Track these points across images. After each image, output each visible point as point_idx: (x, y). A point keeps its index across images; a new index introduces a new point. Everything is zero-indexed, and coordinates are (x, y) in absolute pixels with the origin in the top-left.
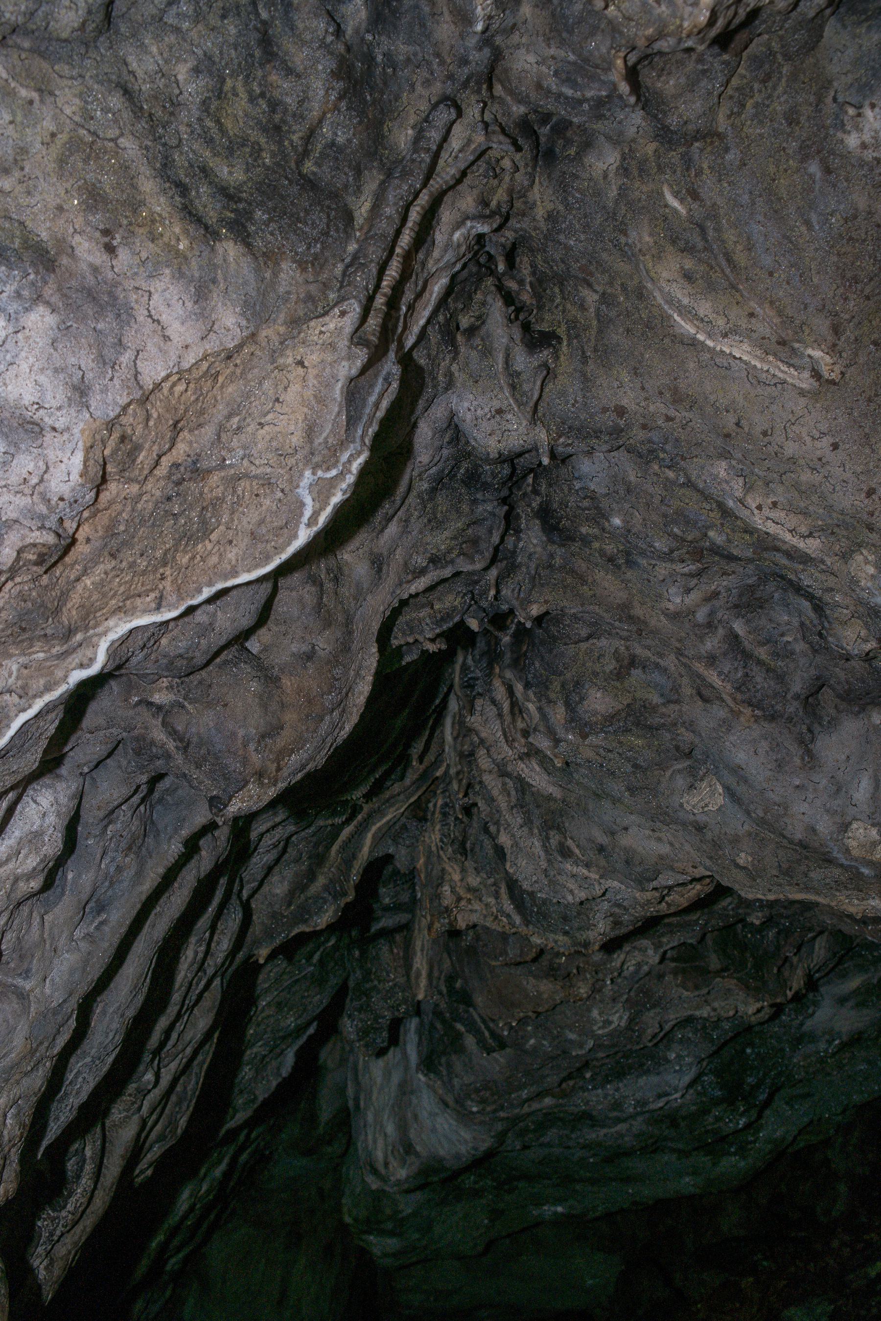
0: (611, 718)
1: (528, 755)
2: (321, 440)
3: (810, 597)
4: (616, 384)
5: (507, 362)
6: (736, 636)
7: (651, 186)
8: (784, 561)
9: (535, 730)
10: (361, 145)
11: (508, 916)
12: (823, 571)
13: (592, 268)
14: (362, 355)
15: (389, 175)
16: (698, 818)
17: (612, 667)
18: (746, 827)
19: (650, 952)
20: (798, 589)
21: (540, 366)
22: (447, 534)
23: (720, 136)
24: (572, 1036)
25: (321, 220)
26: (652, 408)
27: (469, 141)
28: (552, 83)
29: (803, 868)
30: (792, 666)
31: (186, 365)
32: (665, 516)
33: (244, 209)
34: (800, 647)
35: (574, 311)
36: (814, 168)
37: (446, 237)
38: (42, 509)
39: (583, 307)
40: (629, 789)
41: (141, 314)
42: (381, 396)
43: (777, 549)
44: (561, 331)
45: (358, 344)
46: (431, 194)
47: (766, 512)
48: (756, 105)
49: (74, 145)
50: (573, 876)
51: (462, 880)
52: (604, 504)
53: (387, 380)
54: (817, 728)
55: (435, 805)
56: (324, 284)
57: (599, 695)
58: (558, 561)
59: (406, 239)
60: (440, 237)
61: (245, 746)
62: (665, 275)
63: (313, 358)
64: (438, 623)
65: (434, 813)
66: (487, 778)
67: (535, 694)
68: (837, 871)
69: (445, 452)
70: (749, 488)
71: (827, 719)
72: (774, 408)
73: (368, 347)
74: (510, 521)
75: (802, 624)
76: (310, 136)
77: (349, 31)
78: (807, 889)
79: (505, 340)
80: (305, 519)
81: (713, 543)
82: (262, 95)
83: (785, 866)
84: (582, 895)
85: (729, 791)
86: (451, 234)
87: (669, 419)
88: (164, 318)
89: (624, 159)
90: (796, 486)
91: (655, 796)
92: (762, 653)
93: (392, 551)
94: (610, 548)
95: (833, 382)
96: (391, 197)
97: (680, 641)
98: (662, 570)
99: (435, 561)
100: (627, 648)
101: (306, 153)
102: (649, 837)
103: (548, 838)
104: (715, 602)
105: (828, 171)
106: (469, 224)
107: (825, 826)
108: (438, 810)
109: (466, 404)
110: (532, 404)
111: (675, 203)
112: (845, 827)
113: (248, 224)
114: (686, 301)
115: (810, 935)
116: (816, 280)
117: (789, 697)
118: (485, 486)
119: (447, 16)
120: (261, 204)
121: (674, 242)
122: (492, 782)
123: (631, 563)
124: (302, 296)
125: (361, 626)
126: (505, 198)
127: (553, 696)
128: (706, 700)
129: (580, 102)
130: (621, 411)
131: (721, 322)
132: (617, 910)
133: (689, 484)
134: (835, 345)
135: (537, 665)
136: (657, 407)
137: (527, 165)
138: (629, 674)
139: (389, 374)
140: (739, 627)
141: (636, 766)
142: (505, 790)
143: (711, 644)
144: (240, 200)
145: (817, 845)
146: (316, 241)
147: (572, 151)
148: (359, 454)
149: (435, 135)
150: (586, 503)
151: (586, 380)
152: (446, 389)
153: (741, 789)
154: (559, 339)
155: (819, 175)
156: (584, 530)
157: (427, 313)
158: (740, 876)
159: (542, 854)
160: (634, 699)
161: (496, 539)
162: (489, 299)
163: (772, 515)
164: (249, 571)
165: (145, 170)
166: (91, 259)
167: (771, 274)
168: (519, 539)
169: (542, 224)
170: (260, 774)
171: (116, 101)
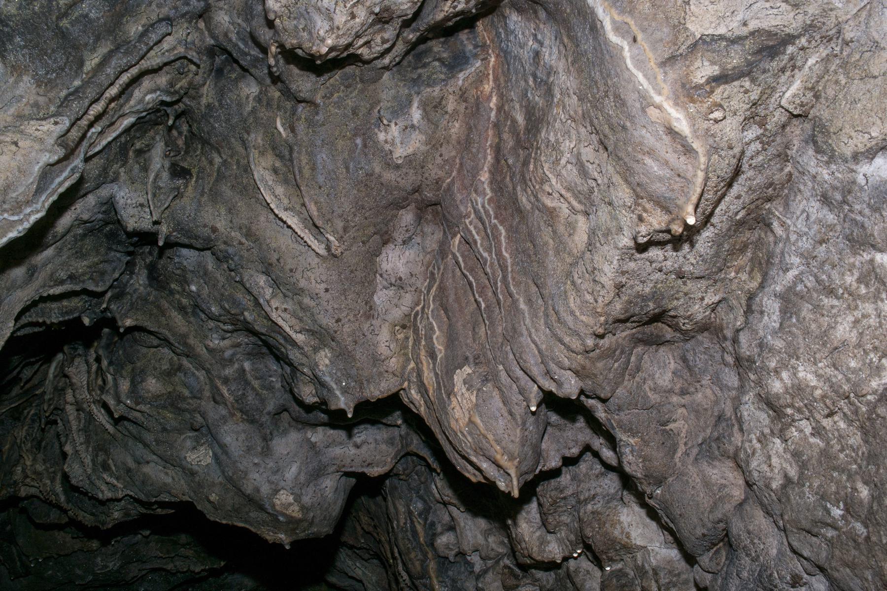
0: (157, 397)
2: (14, 195)
4: (217, 213)
5: (155, 179)
6: (244, 371)
7: (271, 114)
8: (282, 341)
10: (105, 24)
12: (302, 354)
13: (224, 144)
14: (61, 152)
15: (118, 48)
16: (194, 467)
17: (166, 367)
18: (220, 479)
21: (174, 188)
22: (85, 263)
23: (316, 105)
24: (79, 572)
25: (62, 59)
26: (233, 234)
27: (174, 48)
28: (234, 37)
29: (247, 509)
30: (271, 395)
32: (222, 295)
33: (8, 33)
35: (204, 162)
36: (359, 141)
37: (142, 95)
39: (211, 163)
40: (156, 440)
42: (66, 179)
44: (194, 171)
45: (60, 145)
46: (140, 69)
47: (279, 312)
48: (339, 97)
50: (107, 483)
51: (32, 466)
52: (189, 276)
53: (73, 171)
54: (275, 433)
55: (28, 413)
56: (50, 99)
57: (154, 381)
58: (151, 298)
59: (113, 91)
60: (137, 94)
65: (25, 418)
67: (114, 370)
68: (265, 516)
69: (100, 216)
70: (274, 296)
71: (282, 428)
72: (300, 258)
73: (66, 149)
74: (130, 265)
78: (246, 522)
79: (159, 166)
83: (237, 506)
86: (146, 95)
87: (241, 243)
89: (260, 93)
90: (300, 303)
91: (171, 449)
92: (256, 384)
93: (45, 265)
94: (185, 301)
95: (335, 256)
96: (114, 62)
97: (211, 365)
99: (72, 277)
101: (65, 15)
103: (97, 456)
104: (237, 349)
106: (158, 93)
107: (265, 489)
108: (29, 416)
109: (122, 194)
110: (163, 208)
111: (281, 129)
112: (276, 491)
113: (8, 44)
116: (342, 200)
117: (265, 412)
118: (120, 243)
120: (22, 34)
121: (274, 149)
122: (70, 409)
124: (32, 102)
125: (6, 308)
126: (186, 85)
129: (246, 54)
130: (214, 230)
131: (286, 201)
133: (241, 282)
134: (342, 237)
135: (121, 352)
137: (204, 73)
138: (175, 375)
139: (76, 167)
140: (247, 365)
143: (228, 371)
144: (7, 25)
145: (258, 499)
146: (54, 71)
147: (233, 76)
148: (38, 212)
149: (154, 37)
150: (178, 272)
152: (112, 181)
153: (223, 457)
154: (191, 175)
155: (360, 146)
156: (173, 286)
157: (114, 135)
158: (209, 506)
159: (91, 464)
160: (174, 390)
162: (158, 138)
163: (282, 315)
167: (320, 187)
168: (131, 278)
169: (203, 108)
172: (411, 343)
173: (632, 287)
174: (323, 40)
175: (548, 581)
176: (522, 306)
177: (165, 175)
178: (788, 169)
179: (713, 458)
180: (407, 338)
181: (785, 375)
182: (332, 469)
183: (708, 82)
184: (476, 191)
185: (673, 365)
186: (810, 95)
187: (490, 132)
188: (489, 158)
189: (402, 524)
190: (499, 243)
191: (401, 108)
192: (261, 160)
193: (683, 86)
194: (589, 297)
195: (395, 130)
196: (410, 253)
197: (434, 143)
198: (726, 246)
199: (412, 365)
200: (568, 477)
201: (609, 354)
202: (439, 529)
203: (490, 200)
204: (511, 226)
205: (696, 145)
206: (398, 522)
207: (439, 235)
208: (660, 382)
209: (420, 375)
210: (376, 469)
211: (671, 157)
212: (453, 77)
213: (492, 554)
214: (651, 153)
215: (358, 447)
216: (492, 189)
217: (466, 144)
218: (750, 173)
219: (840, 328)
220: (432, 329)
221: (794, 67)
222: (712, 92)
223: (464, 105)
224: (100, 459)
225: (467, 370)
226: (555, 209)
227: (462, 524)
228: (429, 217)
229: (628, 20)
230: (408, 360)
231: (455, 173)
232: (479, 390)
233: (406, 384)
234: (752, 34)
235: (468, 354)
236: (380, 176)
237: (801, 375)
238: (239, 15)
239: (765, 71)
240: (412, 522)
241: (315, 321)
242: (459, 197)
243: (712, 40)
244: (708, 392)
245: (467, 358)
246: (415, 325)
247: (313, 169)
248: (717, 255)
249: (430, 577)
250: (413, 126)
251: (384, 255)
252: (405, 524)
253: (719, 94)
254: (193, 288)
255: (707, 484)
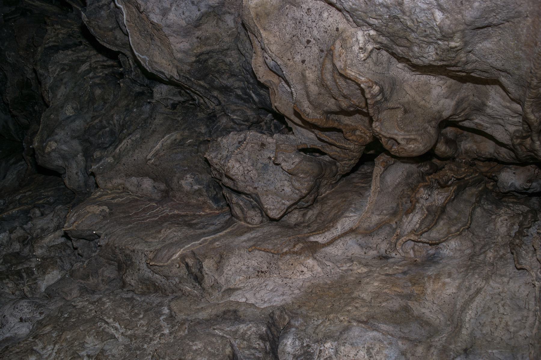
0: (93, 93)
1: (91, 67)
3: (108, 147)
6: (105, 128)
8: (116, 144)
9: (95, 74)
11: (48, 43)
19: (31, 76)
20: (110, 145)
24: (6, 44)
26: (153, 125)
31: (171, 45)
32: (132, 121)
34: (100, 141)
35: (178, 114)
36: (186, 168)
38: (148, 10)
39: (179, 116)
41: (183, 40)
43: (119, 143)
44: (175, 111)
47: (127, 143)
48: (201, 160)
49: (218, 38)
61: (97, 21)
62: (178, 136)
63: (170, 67)
64: (123, 62)
66: (88, 52)
70: (132, 140)
75: (104, 143)
76: (216, 77)
77: (236, 90)
80: (139, 55)
81: (124, 130)
82: (225, 71)
84: (50, 70)
85: (70, 117)
88: (182, 44)
89: (202, 133)
90: (130, 150)
92: (101, 133)
94: (131, 106)
96: (201, 89)
98: (122, 117)
100: (109, 102)
101: (213, 75)
102: (62, 94)
103: (67, 66)
105: (185, 170)
107: (57, 137)
111: (189, 141)
112: (56, 142)
114: (171, 138)
115: (29, 120)
119: (235, 108)
121: (183, 139)
123: (126, 110)
127: (102, 81)
128: (93, 117)
130: (155, 119)
131: (165, 144)
132: (44, 77)
133: (137, 129)
136: (153, 126)
140: (107, 129)
141: (80, 96)
142: (84, 56)
143: (104, 122)
151: (162, 113)
156: (136, 102)
159: (63, 62)
161: (138, 82)
164: (132, 40)
165: (212, 49)
166: (197, 33)
168: (138, 86)
170: (89, 22)
171: (225, 47)
172: (117, 191)
173: (134, 255)
174: (209, 156)
175: (23, 253)
176: (129, 226)
177: (172, 102)
178: (170, 295)
179: (80, 290)
180: (119, 190)
181: (108, 300)
182: (66, 163)
183: (186, 262)
184: (171, 209)
185: (112, 276)
186: (188, 294)
187: (192, 213)
188: (183, 213)
189: (43, 194)
190: (152, 218)
191: (198, 181)
192: (179, 135)
193: (185, 256)
194: (130, 243)
195: (190, 180)
196: (150, 188)
197: (187, 194)
198: (148, 282)
199: (109, 192)
200: (69, 253)
201: (114, 253)
202: (42, 210)
203: (168, 214)
204: (158, 221)
205: (169, 261)
206: (44, 192)
207: (157, 198)
208: (106, 272)
209: (106, 195)
210: (67, 181)
211: (167, 256)
212: (210, 199)
213: (32, 231)
214: (169, 251)
215: (77, 174)
216: (172, 215)
217: (188, 205)
218: (168, 284)
219: (122, 310)
220: (122, 198)
221: (194, 287)
222: (183, 263)
223: (202, 203)
224: (66, 67)
225: (108, 210)
226: (161, 232)
227: (45, 219)
228: (164, 195)
229: (207, 243)
230: (111, 190)
231: (178, 202)
232: (100, 214)
233: (102, 190)
234: (203, 275)
235: (113, 210)
236: (175, 176)
237: (108, 304)
238: (224, 126)
239: (190, 278)
240: (44, 198)
241: (123, 156)
242: (169, 204)
243: (200, 265)
244: (103, 288)
245: (112, 210)
246: (124, 192)
247: (176, 153)
248: (145, 280)
249: (20, 207)
250: (192, 186)
251: (149, 179)
252: (43, 195)
253: (183, 265)
254: (135, 110)
255: (71, 290)
